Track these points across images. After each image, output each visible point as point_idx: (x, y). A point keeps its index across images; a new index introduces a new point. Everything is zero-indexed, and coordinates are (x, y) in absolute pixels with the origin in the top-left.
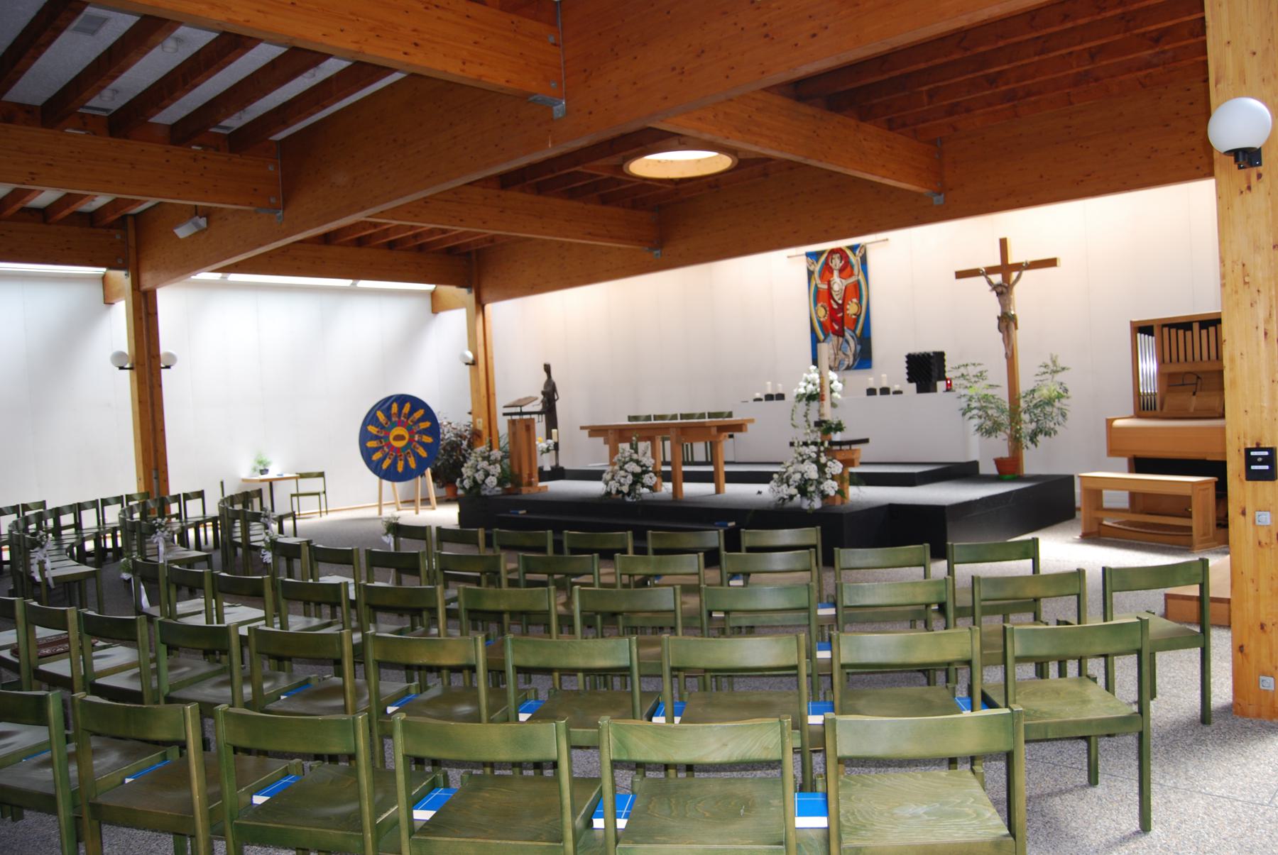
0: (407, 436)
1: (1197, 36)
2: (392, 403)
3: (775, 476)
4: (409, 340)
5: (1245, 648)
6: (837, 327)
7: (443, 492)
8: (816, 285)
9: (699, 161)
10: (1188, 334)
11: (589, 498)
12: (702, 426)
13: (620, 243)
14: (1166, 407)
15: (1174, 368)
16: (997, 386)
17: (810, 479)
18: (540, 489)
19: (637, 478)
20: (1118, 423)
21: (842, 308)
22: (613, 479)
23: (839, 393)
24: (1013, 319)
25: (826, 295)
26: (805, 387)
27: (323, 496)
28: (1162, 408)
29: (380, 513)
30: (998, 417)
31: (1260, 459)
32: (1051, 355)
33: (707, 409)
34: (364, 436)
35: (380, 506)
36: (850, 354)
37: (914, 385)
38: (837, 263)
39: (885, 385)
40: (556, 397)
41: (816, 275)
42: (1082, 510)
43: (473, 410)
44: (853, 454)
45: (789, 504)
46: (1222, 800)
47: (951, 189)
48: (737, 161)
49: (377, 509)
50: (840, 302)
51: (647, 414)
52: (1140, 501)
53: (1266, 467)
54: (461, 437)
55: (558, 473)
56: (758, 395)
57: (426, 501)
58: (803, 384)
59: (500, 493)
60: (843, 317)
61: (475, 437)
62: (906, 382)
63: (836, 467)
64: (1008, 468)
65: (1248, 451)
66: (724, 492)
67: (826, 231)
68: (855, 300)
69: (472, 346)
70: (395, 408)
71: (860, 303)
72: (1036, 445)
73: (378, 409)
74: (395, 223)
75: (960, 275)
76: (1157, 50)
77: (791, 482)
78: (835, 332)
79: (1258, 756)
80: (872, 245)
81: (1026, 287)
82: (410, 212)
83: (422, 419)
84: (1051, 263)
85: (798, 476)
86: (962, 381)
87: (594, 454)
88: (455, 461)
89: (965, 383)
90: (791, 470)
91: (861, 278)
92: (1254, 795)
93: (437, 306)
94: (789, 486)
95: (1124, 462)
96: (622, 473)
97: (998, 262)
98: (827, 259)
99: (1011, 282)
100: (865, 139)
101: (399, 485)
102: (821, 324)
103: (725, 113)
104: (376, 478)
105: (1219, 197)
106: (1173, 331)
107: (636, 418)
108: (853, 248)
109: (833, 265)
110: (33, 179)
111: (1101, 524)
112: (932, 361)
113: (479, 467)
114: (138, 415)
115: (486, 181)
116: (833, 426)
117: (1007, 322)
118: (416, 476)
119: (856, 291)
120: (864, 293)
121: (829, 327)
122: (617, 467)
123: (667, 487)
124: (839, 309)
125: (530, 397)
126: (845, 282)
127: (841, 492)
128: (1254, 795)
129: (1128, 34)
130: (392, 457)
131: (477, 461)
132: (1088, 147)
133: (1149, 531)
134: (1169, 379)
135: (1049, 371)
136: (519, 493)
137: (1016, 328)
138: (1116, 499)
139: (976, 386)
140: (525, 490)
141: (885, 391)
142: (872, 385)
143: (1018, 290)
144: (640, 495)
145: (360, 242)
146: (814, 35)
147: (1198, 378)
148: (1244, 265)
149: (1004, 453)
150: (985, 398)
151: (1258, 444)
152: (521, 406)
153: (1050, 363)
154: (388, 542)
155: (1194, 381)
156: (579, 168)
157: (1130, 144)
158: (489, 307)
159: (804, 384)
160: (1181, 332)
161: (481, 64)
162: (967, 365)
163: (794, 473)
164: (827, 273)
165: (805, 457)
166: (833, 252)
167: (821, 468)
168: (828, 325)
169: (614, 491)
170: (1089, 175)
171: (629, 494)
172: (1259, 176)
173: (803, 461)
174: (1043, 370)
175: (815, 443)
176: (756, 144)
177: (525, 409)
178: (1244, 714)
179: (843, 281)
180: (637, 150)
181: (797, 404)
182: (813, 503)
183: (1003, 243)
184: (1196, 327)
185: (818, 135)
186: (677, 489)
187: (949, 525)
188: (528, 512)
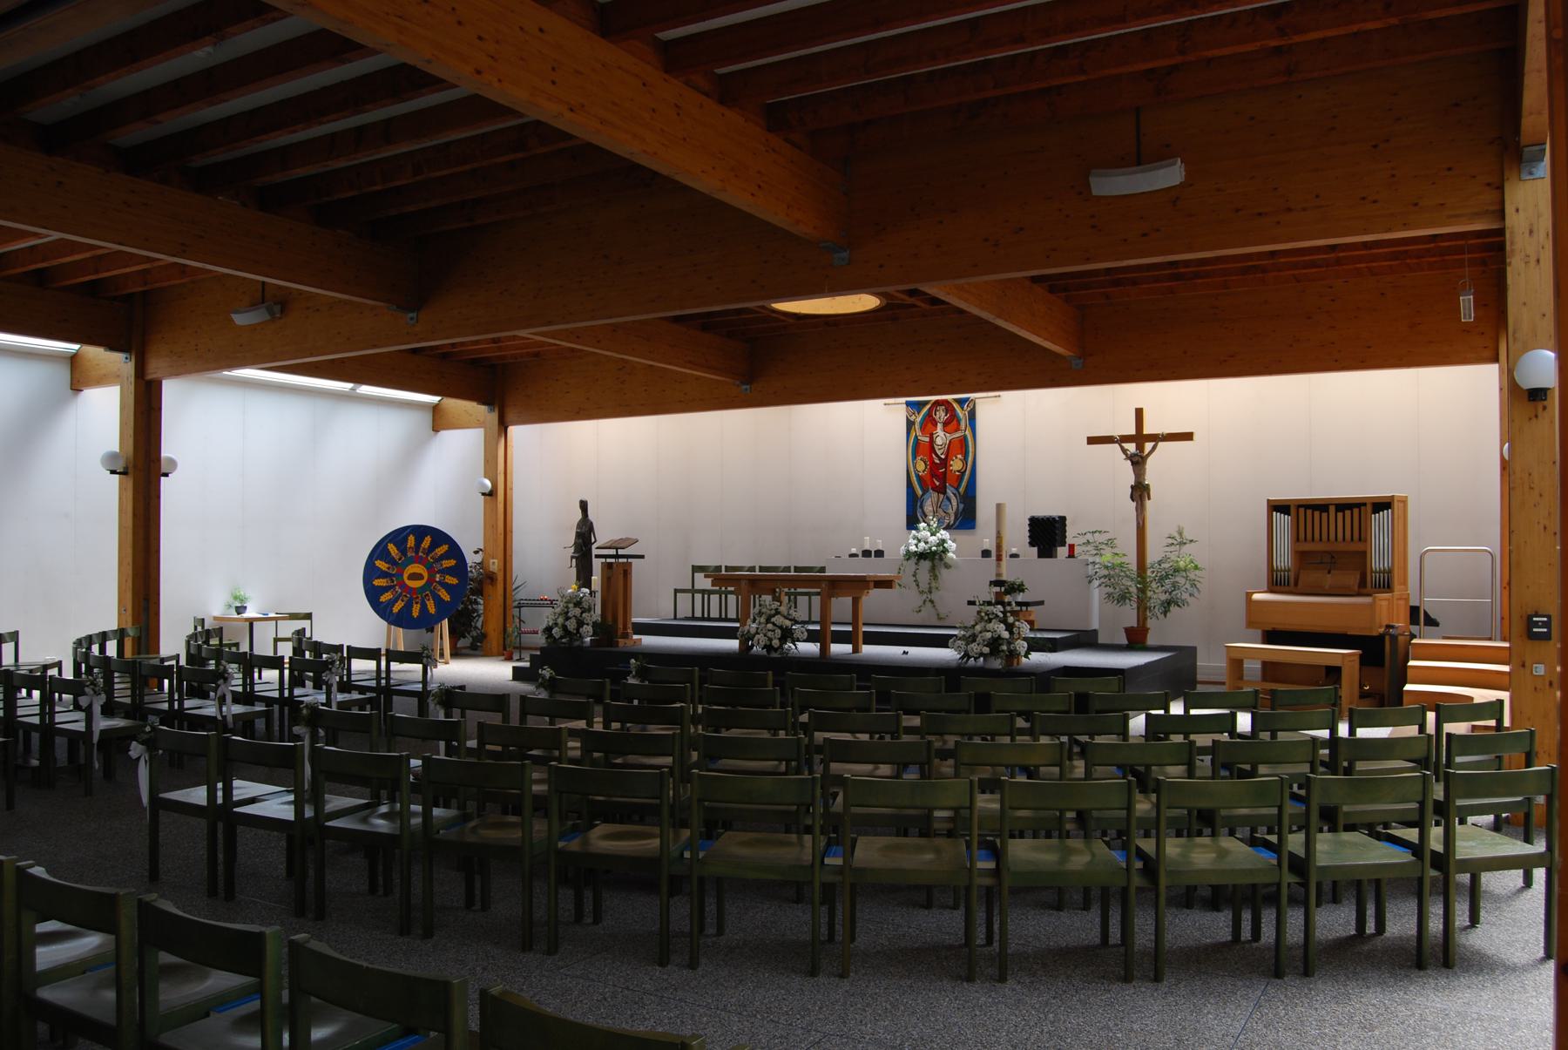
2: (408, 535)
4: (407, 460)
6: (938, 484)
8: (916, 436)
11: (712, 653)
14: (1300, 583)
18: (635, 641)
20: (1256, 597)
21: (945, 463)
23: (953, 552)
24: (1147, 488)
26: (916, 545)
31: (1540, 624)
32: (1179, 527)
34: (370, 572)
36: (952, 512)
37: (1035, 549)
38: (941, 415)
40: (593, 540)
42: (1227, 684)
44: (1030, 615)
50: (943, 457)
52: (1272, 669)
53: (1545, 630)
56: (854, 550)
60: (945, 473)
62: (1028, 545)
65: (1530, 617)
66: (861, 652)
68: (959, 456)
69: (490, 471)
70: (411, 541)
71: (965, 460)
75: (1092, 441)
78: (935, 489)
80: (981, 400)
81: (1161, 460)
83: (445, 556)
84: (1188, 436)
93: (439, 420)
97: (1133, 431)
106: (1309, 512)
108: (961, 402)
109: (937, 418)
110: (184, 251)
112: (1057, 525)
114: (130, 532)
116: (1016, 586)
117: (1140, 492)
119: (963, 447)
121: (929, 482)
123: (811, 648)
124: (941, 464)
125: (627, 539)
130: (405, 599)
134: (1303, 558)
137: (1149, 499)
140: (621, 642)
143: (1151, 463)
146: (1144, 235)
148: (1530, 475)
151: (1536, 612)
159: (915, 542)
160: (1317, 514)
166: (937, 403)
167: (1010, 627)
170: (1232, 356)
172: (1545, 408)
173: (990, 621)
174: (1171, 541)
177: (621, 552)
179: (948, 435)
181: (905, 562)
183: (1139, 413)
184: (1332, 509)
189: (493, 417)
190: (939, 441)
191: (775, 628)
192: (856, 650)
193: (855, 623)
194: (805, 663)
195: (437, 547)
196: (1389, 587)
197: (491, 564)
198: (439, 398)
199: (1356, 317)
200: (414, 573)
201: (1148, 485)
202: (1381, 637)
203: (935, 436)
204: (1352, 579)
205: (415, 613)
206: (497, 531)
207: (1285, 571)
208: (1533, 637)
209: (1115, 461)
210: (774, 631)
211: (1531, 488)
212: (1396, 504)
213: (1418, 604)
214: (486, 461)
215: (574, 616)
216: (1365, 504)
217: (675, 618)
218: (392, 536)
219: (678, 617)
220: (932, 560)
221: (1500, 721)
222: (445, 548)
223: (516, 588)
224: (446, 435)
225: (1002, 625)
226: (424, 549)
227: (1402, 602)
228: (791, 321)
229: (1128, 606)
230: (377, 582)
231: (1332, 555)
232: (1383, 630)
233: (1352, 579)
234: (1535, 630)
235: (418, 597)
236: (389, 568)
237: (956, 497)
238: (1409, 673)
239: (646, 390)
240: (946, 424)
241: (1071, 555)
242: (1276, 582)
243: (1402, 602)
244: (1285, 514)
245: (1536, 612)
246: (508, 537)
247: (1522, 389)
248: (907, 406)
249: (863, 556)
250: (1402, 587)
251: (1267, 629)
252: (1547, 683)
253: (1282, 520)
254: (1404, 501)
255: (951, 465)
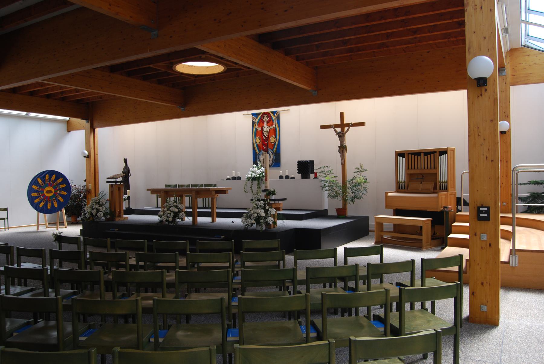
0: (53, 191)
1: (431, 33)
2: (46, 174)
3: (244, 214)
5: (475, 293)
6: (265, 148)
7: (70, 219)
8: (256, 128)
9: (208, 67)
10: (419, 157)
11: (151, 224)
12: (208, 191)
13: (165, 103)
15: (412, 172)
16: (337, 177)
17: (261, 216)
18: (124, 218)
19: (176, 215)
20: (390, 194)
21: (268, 139)
22: (164, 215)
25: (260, 134)
26: (251, 174)
27: (6, 220)
28: (407, 189)
29: (38, 229)
30: (338, 190)
31: (484, 212)
33: (190, 183)
34: (30, 190)
35: (38, 226)
38: (266, 119)
39: (287, 174)
40: (129, 175)
41: (256, 124)
42: (375, 231)
43: (87, 179)
44: (279, 205)
45: (250, 228)
46: (481, 362)
47: (320, 89)
48: (226, 69)
49: (36, 227)
50: (267, 136)
51: (175, 184)
52: (398, 228)
54: (80, 192)
55: (130, 211)
56: (228, 177)
57: (62, 223)
58: (250, 173)
59: (104, 220)
60: (268, 143)
61: (87, 193)
63: (273, 211)
64: (341, 214)
65: (479, 208)
66: (216, 222)
67: (263, 104)
68: (273, 136)
69: (88, 148)
72: (354, 203)
73: (38, 177)
74: (56, 84)
75: (323, 127)
76: (415, 36)
77: (252, 217)
78: (264, 150)
79: (487, 341)
81: (351, 134)
82: (64, 80)
83: (62, 183)
84: (362, 124)
85: (256, 215)
86: (321, 174)
87: (153, 203)
88: (77, 203)
89: (324, 175)
90: (252, 212)
91: (277, 126)
92: (493, 359)
93: (69, 127)
94: (251, 219)
95: (391, 211)
96: (169, 212)
97: (339, 123)
98: (261, 116)
99: (345, 132)
100: (287, 64)
101: (47, 215)
102: (258, 146)
103: (229, 45)
104: (36, 212)
105: (468, 98)
107: (169, 186)
108: (274, 113)
111: (382, 238)
113: (94, 208)
115: (103, 69)
116: (271, 192)
117: (342, 149)
118: (58, 211)
119: (275, 132)
120: (278, 133)
121: (261, 148)
122: (166, 209)
123: (188, 220)
126: (269, 128)
127: (275, 223)
128: (493, 359)
129: (405, 28)
131: (93, 204)
132: (380, 76)
133: (413, 242)
134: (411, 177)
135: (359, 171)
136: (114, 220)
137: (346, 152)
138: (388, 226)
139: (328, 176)
140: (117, 219)
141: (287, 177)
142: (281, 174)
143: (347, 136)
144: (177, 222)
145: (32, 94)
146: (286, 11)
147: (423, 176)
148: (478, 128)
149: (341, 206)
150: (333, 182)
151: (482, 205)
152: (116, 178)
153: (360, 168)
154: (56, 245)
155: (421, 178)
156: (151, 66)
157: (397, 76)
158: (97, 130)
159: (251, 173)
160: (416, 157)
161: (118, 7)
162: (324, 167)
163: (253, 213)
164: (261, 123)
165: (258, 206)
166: (264, 114)
167: (266, 211)
168: (261, 146)
169: (164, 220)
171: (171, 222)
172: (486, 90)
173: (258, 208)
174: (357, 170)
175: (263, 200)
176: (242, 60)
178: (474, 322)
179: (268, 127)
180: (181, 59)
181: (247, 182)
182: (262, 227)
183: (342, 114)
184: (422, 154)
185: (268, 60)
186: (195, 220)
187: (322, 237)
188: (119, 230)
189: (88, 125)
190: (265, 130)
191: (171, 212)
192: (213, 221)
193: (212, 208)
194: (186, 229)
195: (58, 179)
196: (446, 189)
197: (89, 185)
198: (69, 118)
199: (433, 68)
200: (48, 190)
201: (346, 146)
202: (442, 212)
203: (263, 128)
204: (431, 186)
205: (49, 207)
206: (91, 171)
207: (444, 182)
208: (480, 219)
209: (331, 135)
210: (170, 214)
211: (479, 136)
212: (449, 152)
213: (460, 196)
214: (86, 143)
215: (95, 208)
216: (436, 152)
217: (157, 207)
218: (41, 173)
219: (158, 207)
220: (258, 181)
221: (460, 267)
222: (61, 179)
223: (105, 195)
224: (73, 133)
225: (263, 210)
226: (53, 180)
227: (452, 196)
228: (192, 78)
229: (336, 199)
230: (33, 195)
231: (423, 175)
232: (442, 209)
233: (431, 186)
234: (481, 215)
235: (50, 201)
236: (38, 189)
237: (272, 154)
238: (453, 229)
239: (145, 112)
240: (268, 122)
241: (316, 177)
242: (400, 188)
243: (452, 196)
244: (399, 156)
245: (482, 205)
246: (97, 174)
247: (470, 78)
248: (252, 115)
249: (232, 180)
250: (453, 189)
251: (394, 209)
252: (488, 245)
253: (402, 160)
254: (453, 150)
255: (270, 140)
